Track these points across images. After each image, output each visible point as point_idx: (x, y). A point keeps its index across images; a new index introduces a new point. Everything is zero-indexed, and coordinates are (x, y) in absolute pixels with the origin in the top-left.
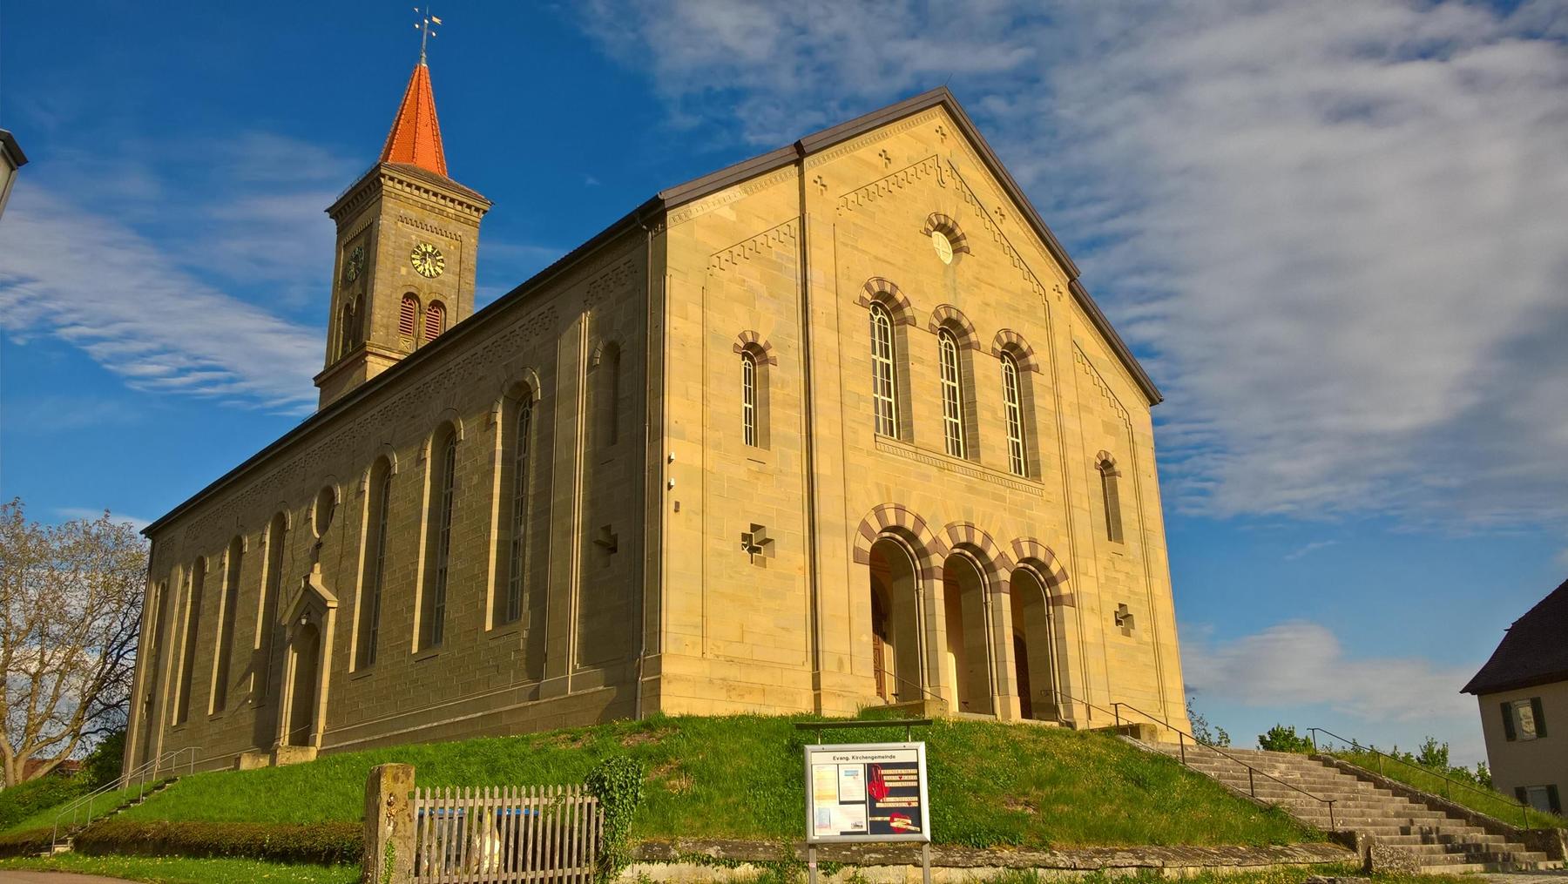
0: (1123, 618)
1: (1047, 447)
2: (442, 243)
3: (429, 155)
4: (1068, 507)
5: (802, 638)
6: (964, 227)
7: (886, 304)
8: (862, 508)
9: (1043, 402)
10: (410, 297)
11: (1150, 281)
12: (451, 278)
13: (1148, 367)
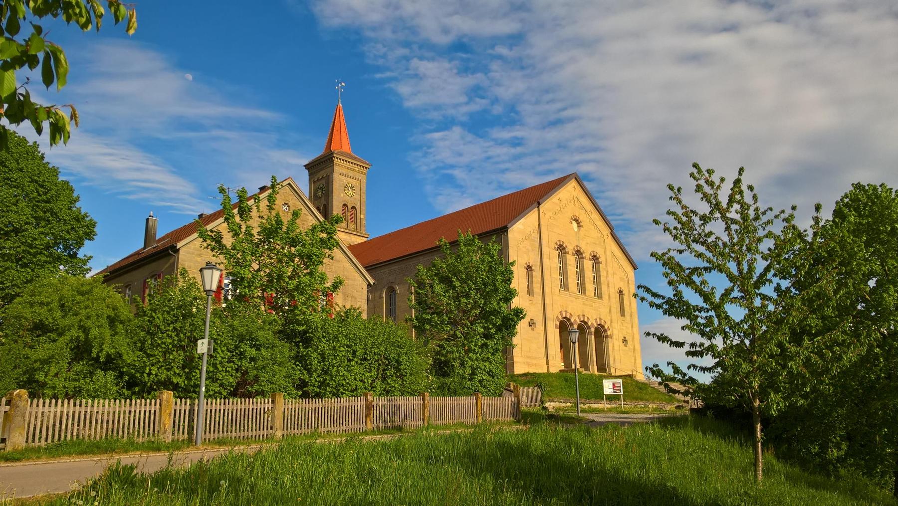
0: (625, 341)
1: (604, 288)
2: (354, 182)
3: (346, 147)
4: (610, 307)
5: (543, 350)
6: (581, 219)
7: (561, 248)
8: (557, 313)
9: (603, 273)
10: (345, 205)
11: (589, 142)
12: (357, 197)
13: (589, 186)
